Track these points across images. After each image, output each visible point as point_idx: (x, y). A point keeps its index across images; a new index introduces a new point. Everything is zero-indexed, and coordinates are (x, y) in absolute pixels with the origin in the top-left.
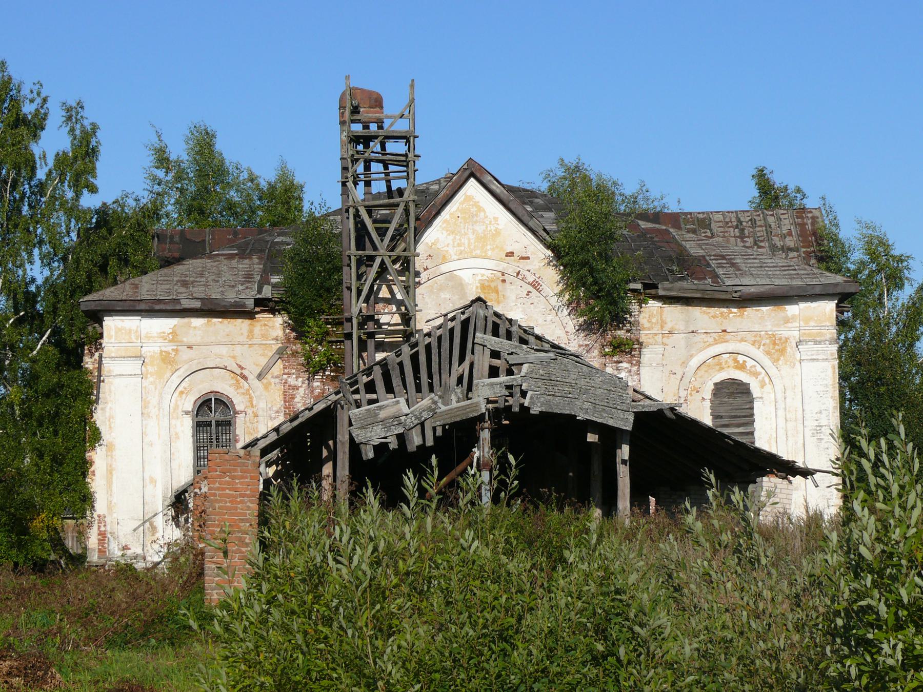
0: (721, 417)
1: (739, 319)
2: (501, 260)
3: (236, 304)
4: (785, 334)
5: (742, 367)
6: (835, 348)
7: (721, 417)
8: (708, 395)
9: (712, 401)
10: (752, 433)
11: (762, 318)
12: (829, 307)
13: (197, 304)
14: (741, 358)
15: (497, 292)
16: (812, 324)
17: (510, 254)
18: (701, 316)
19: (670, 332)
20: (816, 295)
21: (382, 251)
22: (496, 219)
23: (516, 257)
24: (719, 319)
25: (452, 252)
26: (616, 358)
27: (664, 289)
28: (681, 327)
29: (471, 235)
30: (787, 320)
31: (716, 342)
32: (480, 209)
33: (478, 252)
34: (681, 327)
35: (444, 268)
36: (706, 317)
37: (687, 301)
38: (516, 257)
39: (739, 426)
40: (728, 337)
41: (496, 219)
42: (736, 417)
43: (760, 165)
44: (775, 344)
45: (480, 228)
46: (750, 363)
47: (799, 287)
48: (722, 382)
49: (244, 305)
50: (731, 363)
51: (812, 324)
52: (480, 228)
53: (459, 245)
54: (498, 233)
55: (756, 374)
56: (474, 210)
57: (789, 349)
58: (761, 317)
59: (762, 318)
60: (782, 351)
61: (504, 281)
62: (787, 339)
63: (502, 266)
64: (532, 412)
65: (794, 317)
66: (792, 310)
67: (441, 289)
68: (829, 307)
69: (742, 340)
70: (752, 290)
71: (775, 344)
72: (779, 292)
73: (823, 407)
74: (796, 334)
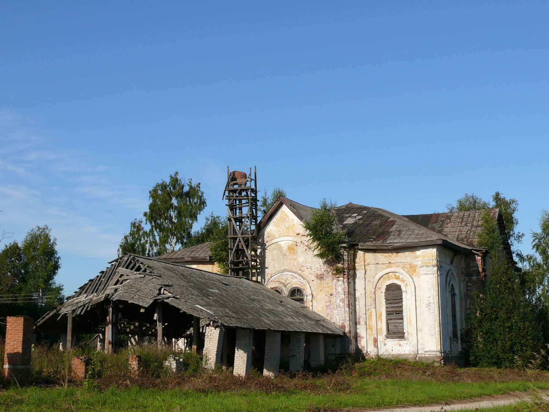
0: (389, 300)
1: (396, 257)
2: (295, 237)
3: (203, 259)
4: (416, 263)
5: (398, 278)
6: (436, 268)
7: (389, 300)
8: (384, 291)
9: (385, 293)
10: (402, 307)
11: (406, 256)
12: (433, 252)
13: (190, 259)
14: (397, 274)
15: (294, 250)
16: (426, 258)
17: (298, 234)
18: (381, 257)
19: (368, 264)
20: (426, 246)
21: (239, 235)
22: (293, 220)
23: (300, 235)
24: (388, 258)
25: (277, 234)
26: (337, 276)
27: (361, 246)
28: (373, 262)
29: (284, 228)
30: (416, 257)
31: (387, 267)
32: (287, 216)
33: (286, 234)
34: (373, 262)
35: (274, 241)
36: (383, 257)
37: (374, 251)
38: (300, 235)
39: (396, 303)
40: (392, 265)
41: (293, 220)
42: (394, 300)
43: (133, 220)
44: (411, 268)
45: (287, 224)
46: (401, 276)
47: (417, 243)
48: (390, 285)
49: (206, 259)
50: (394, 277)
51: (426, 258)
52: (287, 224)
53: (279, 231)
54: (294, 225)
55: (404, 281)
56: (285, 217)
57: (417, 270)
58: (405, 257)
59: (406, 256)
60: (415, 271)
61: (296, 245)
62: (416, 265)
63: (296, 239)
64: (517, 265)
65: (419, 256)
66: (419, 253)
67: (273, 249)
68: (433, 252)
69: (398, 266)
70: (398, 245)
71: (411, 268)
72: (408, 245)
73: (431, 295)
74: (420, 263)
